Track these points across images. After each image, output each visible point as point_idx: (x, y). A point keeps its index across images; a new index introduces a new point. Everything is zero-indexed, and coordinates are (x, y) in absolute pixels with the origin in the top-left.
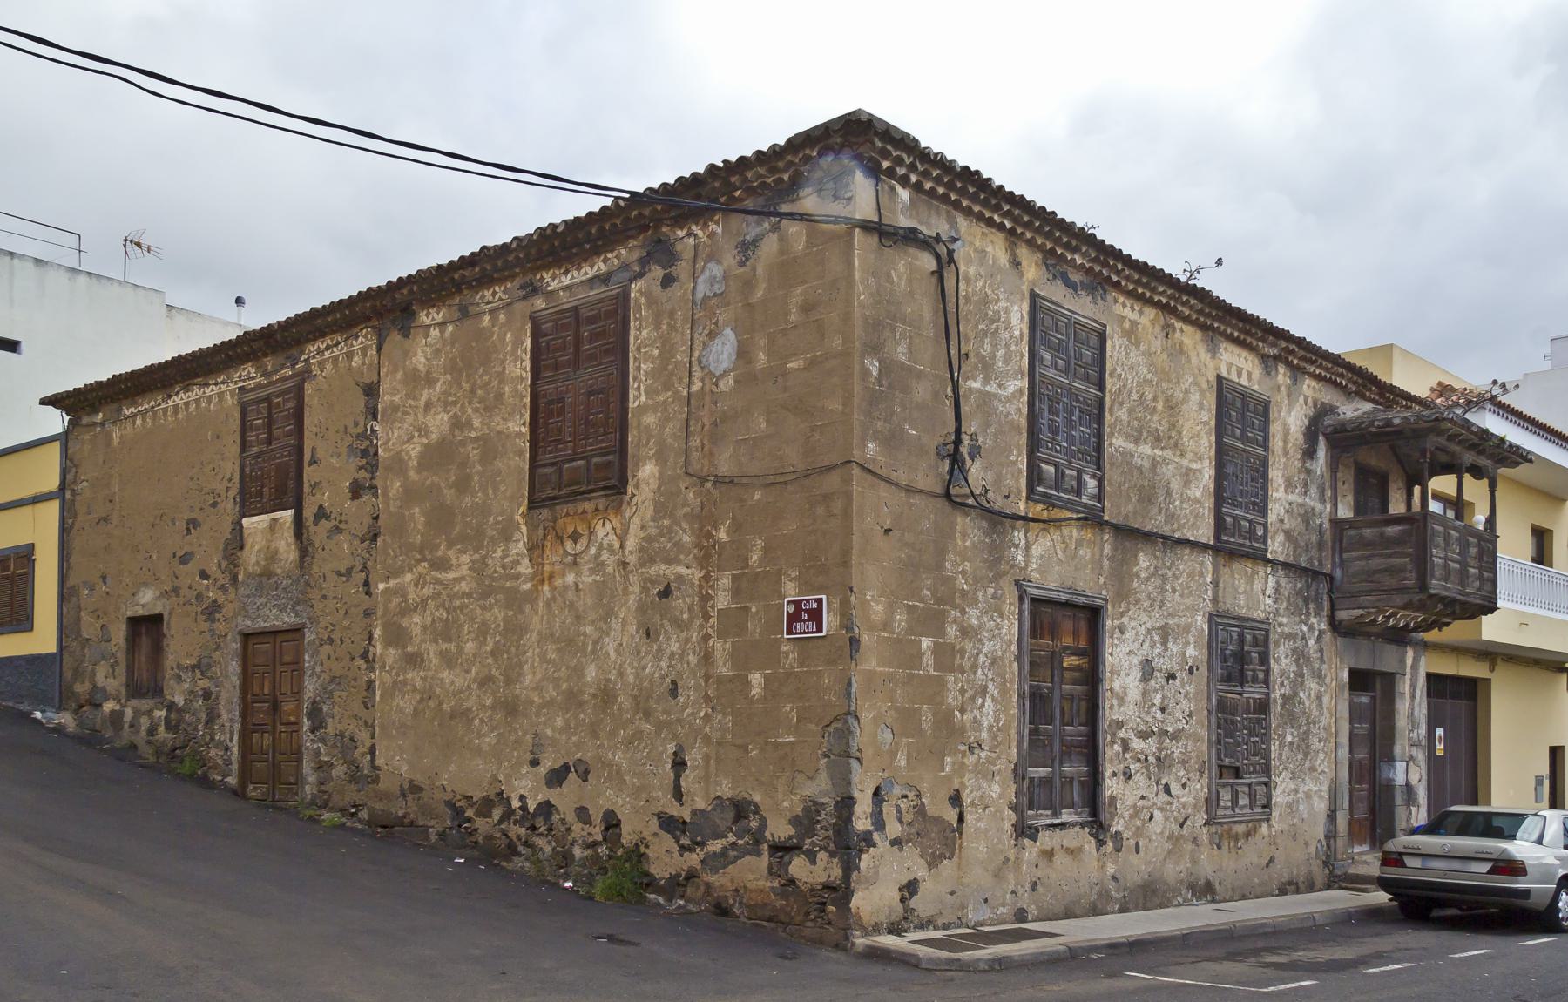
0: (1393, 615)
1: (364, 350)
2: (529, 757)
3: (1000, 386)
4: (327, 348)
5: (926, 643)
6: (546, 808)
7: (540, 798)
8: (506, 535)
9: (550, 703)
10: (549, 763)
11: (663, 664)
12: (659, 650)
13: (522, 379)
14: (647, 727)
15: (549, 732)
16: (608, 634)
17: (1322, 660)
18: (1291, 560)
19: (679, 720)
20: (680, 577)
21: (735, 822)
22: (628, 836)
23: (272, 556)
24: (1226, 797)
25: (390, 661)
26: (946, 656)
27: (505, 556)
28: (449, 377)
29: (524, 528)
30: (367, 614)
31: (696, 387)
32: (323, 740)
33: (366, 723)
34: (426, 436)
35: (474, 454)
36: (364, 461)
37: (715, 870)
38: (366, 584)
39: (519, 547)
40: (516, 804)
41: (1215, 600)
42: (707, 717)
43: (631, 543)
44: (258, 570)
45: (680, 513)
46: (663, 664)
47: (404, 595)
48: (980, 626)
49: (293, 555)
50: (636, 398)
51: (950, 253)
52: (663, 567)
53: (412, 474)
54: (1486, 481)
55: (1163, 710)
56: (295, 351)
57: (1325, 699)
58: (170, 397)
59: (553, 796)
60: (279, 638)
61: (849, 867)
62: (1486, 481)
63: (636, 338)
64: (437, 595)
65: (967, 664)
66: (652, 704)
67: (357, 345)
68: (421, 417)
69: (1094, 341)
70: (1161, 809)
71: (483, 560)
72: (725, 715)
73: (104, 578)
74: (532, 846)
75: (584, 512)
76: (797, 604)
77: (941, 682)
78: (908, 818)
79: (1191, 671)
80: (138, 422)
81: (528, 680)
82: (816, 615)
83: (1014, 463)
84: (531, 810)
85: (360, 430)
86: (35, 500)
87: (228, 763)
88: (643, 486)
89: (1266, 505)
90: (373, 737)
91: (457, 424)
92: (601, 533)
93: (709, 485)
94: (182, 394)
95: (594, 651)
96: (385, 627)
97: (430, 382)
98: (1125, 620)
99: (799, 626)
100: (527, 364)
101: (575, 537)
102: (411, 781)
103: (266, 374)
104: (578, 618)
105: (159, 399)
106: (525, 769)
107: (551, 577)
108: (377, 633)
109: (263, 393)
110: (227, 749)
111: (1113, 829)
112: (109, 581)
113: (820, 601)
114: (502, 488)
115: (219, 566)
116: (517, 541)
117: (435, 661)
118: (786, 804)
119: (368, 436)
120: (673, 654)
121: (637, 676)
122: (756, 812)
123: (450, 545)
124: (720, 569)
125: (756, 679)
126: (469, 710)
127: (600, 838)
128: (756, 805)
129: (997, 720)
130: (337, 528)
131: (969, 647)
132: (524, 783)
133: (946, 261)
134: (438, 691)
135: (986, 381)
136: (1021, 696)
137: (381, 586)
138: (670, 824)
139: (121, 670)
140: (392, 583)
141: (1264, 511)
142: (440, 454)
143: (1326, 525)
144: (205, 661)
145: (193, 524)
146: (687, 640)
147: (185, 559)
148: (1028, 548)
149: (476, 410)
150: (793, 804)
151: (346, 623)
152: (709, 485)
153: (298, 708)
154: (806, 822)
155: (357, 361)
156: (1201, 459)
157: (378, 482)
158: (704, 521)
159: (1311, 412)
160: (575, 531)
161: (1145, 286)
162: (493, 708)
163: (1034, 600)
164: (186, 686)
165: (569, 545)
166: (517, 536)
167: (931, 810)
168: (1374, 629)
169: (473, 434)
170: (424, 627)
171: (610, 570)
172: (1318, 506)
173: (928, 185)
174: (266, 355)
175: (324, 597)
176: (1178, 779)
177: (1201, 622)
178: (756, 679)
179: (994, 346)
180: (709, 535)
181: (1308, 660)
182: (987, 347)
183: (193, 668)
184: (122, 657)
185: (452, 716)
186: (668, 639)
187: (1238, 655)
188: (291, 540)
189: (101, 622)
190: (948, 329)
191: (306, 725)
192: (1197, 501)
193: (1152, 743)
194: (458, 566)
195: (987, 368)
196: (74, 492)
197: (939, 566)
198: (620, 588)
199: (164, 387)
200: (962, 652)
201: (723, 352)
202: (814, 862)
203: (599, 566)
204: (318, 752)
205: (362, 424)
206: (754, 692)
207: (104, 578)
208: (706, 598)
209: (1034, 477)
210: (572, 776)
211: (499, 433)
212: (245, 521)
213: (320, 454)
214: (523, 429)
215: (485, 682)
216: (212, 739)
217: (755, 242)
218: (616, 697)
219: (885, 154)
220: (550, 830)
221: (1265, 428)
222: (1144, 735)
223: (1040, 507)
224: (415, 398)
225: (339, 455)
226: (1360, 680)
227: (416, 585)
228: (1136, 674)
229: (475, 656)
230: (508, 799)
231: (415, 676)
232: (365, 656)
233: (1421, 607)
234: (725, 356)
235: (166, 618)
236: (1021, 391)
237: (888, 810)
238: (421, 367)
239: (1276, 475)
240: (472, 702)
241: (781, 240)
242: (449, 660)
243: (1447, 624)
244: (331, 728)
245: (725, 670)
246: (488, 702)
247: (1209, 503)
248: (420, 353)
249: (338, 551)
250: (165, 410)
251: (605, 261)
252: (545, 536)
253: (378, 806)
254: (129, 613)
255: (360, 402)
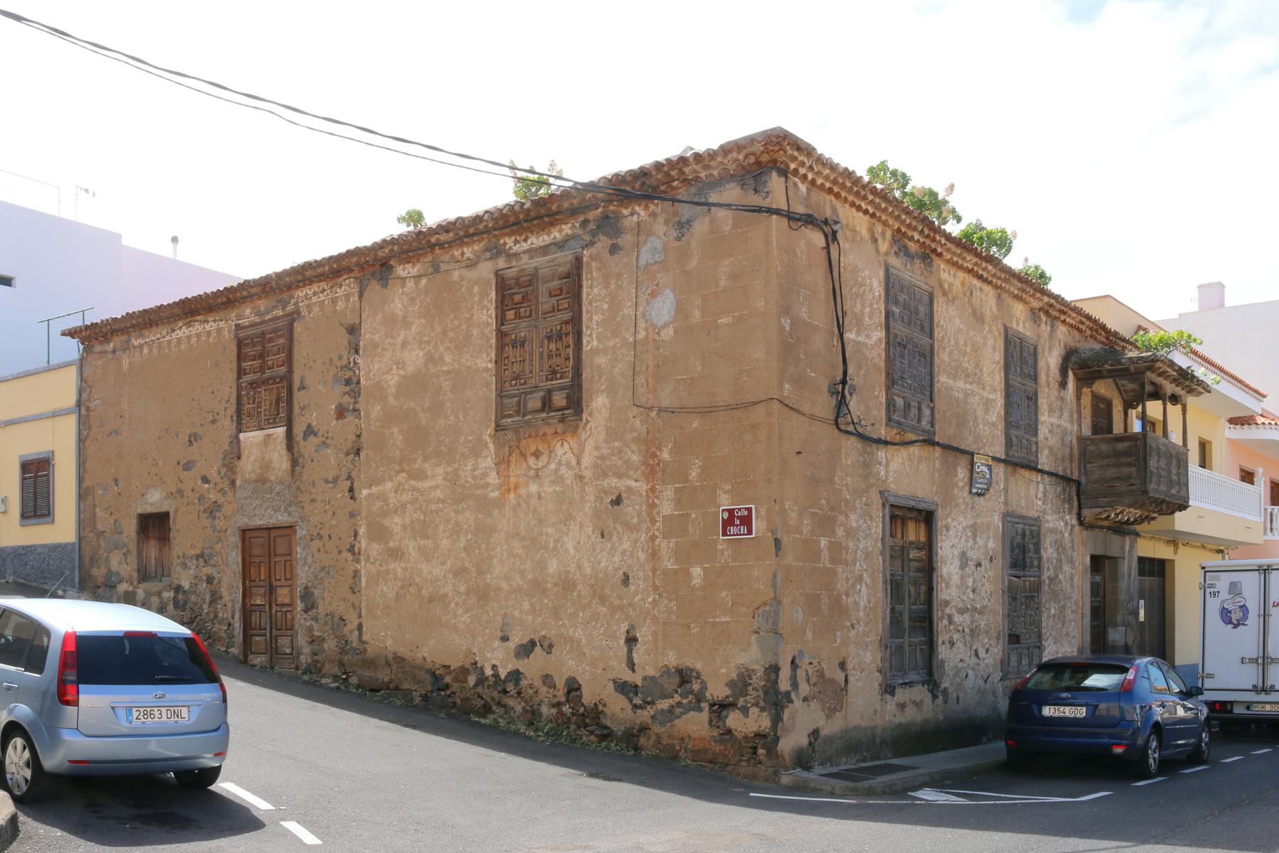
0: (1122, 512)
1: (347, 297)
2: (499, 634)
3: (867, 336)
4: (315, 294)
5: (824, 542)
6: (516, 676)
7: (510, 668)
8: (476, 451)
9: (519, 589)
10: (517, 638)
11: (616, 559)
12: (613, 548)
13: (488, 324)
14: (603, 610)
15: (517, 613)
16: (567, 535)
17: (1073, 548)
18: (1052, 470)
19: (630, 605)
20: (629, 489)
21: (680, 686)
22: (588, 697)
23: (266, 465)
24: (1014, 659)
25: (374, 553)
26: (836, 548)
27: (474, 470)
28: (423, 321)
29: (491, 446)
30: (352, 515)
31: (642, 335)
32: (315, 619)
33: (354, 605)
34: (403, 368)
35: (446, 385)
36: (348, 389)
37: (663, 724)
38: (351, 490)
39: (487, 462)
40: (489, 672)
41: (1006, 503)
42: (655, 603)
43: (587, 460)
44: (254, 476)
45: (629, 437)
46: (616, 559)
47: (385, 500)
48: (859, 527)
49: (286, 465)
50: (588, 342)
51: (834, 233)
52: (615, 480)
53: (391, 399)
54: (1179, 406)
55: (974, 591)
56: (285, 296)
57: (1075, 579)
58: (173, 331)
59: (521, 665)
60: (274, 533)
61: (777, 719)
62: (1179, 406)
63: (588, 294)
64: (414, 501)
65: (850, 558)
66: (607, 591)
67: (340, 292)
68: (398, 353)
69: (926, 299)
70: (973, 669)
71: (456, 471)
72: (670, 600)
73: (116, 480)
74: (504, 706)
75: (545, 434)
76: (731, 512)
77: (833, 573)
78: (813, 680)
79: (991, 560)
80: (146, 351)
81: (498, 570)
82: (747, 521)
83: (877, 397)
84: (503, 677)
85: (345, 362)
86: (55, 414)
87: (232, 637)
88: (597, 415)
89: (1036, 428)
90: (360, 617)
91: (430, 359)
92: (559, 451)
93: (653, 414)
94: (184, 329)
95: (555, 549)
96: (369, 525)
97: (407, 324)
98: (949, 520)
99: (733, 530)
100: (493, 312)
101: (537, 455)
102: (394, 653)
103: (258, 314)
104: (540, 521)
105: (164, 333)
106: (497, 643)
107: (516, 487)
108: (362, 531)
109: (258, 330)
110: (229, 625)
111: (943, 686)
112: (120, 483)
113: (749, 510)
114: (471, 413)
115: (219, 473)
116: (486, 457)
117: (414, 554)
118: (723, 670)
119: (351, 367)
120: (624, 552)
121: (593, 568)
122: (698, 678)
123: (426, 459)
124: (664, 482)
125: (697, 571)
126: (445, 595)
127: (564, 699)
128: (698, 673)
129: (869, 602)
130: (324, 443)
131: (851, 545)
132: (496, 655)
133: (832, 237)
134: (417, 579)
135: (858, 334)
136: (885, 582)
137: (365, 492)
138: (625, 688)
139: (133, 558)
140: (375, 490)
141: (1036, 435)
142: (416, 384)
143: (1074, 442)
144: (207, 552)
145: (193, 438)
146: (636, 541)
147: (188, 466)
148: (887, 465)
149: (448, 349)
150: (728, 671)
151: (334, 522)
152: (653, 414)
153: (292, 593)
154: (741, 684)
155: (340, 305)
156: (995, 391)
157: (360, 406)
158: (650, 445)
159: (1063, 352)
160: (537, 450)
161: (959, 256)
162: (467, 593)
163: (892, 506)
164: (192, 572)
165: (532, 461)
166: (485, 453)
167: (828, 674)
168: (1106, 523)
169: (445, 369)
170: (404, 527)
171: (568, 482)
172: (1068, 426)
173: (819, 182)
174: (260, 298)
175: (313, 500)
176: (983, 645)
177: (997, 521)
178: (697, 571)
179: (863, 305)
180: (654, 455)
181: (1064, 549)
182: (858, 306)
183: (198, 557)
184: (133, 546)
185: (430, 601)
186: (620, 539)
187: (1022, 550)
188: (284, 452)
189: (114, 517)
190: (835, 294)
191: (300, 606)
192: (994, 425)
193: (967, 616)
194: (433, 476)
195: (859, 321)
196: (88, 409)
197: (831, 481)
198: (577, 497)
199: (169, 323)
200: (847, 548)
201: (663, 308)
202: (746, 715)
203: (559, 479)
204: (310, 629)
205: (345, 357)
206: (694, 582)
207: (116, 480)
208: (652, 506)
209: (890, 406)
210: (538, 649)
211: (469, 368)
212: (242, 436)
213: (308, 382)
214: (490, 365)
215: (459, 572)
216: (216, 616)
217: (689, 222)
218: (575, 585)
219: (794, 159)
220: (519, 693)
221: (1035, 367)
222: (962, 612)
223: (895, 431)
224: (392, 337)
225: (325, 383)
226: (1098, 563)
227: (396, 492)
228: (957, 563)
229: (449, 551)
230: (482, 669)
231: (396, 567)
232: (351, 549)
233: (1141, 506)
234: (665, 311)
235: (172, 515)
236: (880, 340)
237: (801, 674)
238: (399, 313)
239: (1043, 402)
240: (448, 589)
241: (711, 221)
242: (426, 554)
243: (1154, 519)
244: (322, 609)
245: (669, 564)
246: (462, 589)
247: (1001, 426)
248: (397, 300)
249: (325, 462)
250: (169, 342)
251: (561, 231)
252: (510, 454)
253: (367, 673)
254: (139, 511)
255: (345, 338)
